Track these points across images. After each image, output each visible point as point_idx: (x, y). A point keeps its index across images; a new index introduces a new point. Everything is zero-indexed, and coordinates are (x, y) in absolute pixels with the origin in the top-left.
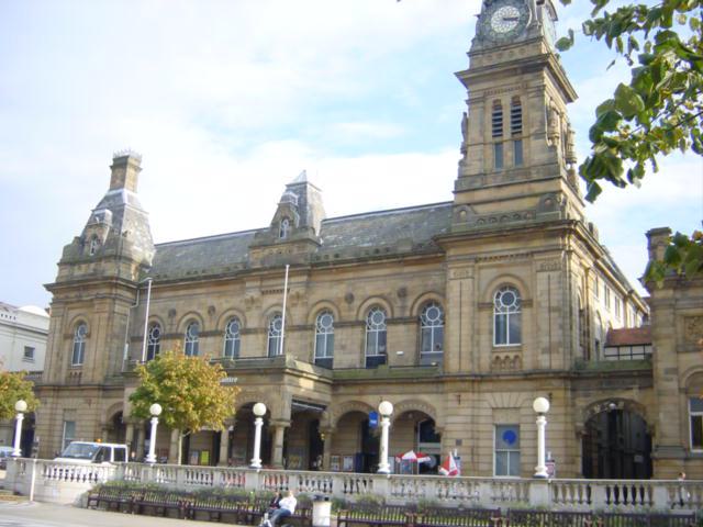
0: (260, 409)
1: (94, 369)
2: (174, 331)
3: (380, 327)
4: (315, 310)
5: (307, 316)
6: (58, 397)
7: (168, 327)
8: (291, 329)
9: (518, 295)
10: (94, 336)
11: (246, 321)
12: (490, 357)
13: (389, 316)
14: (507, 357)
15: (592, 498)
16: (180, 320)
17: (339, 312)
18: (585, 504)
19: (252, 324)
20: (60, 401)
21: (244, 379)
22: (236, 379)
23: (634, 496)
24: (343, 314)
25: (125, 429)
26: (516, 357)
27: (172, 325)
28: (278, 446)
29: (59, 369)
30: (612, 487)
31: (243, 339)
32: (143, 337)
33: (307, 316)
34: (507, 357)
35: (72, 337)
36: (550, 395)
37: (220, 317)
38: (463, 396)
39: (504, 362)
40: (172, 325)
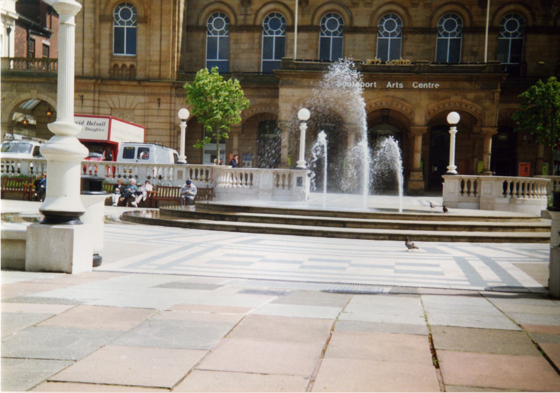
0: (454, 118)
1: (160, 62)
2: (250, 22)
3: (514, 35)
4: (440, 12)
5: (431, 18)
6: (100, 93)
7: (241, 18)
8: (301, 29)
9: (135, 10)
10: (156, 21)
11: (351, 18)
12: (110, 64)
13: (347, 22)
14: (124, 66)
15: (253, 182)
16: (258, 11)
17: (471, 17)
18: (204, 181)
19: (361, 21)
20: (103, 98)
21: (447, 84)
22: (437, 85)
23: (469, 187)
24: (475, 18)
25: (413, 138)
26: (132, 66)
27: (246, 15)
28: (285, 147)
29: (96, 59)
30: (111, 166)
31: (348, 37)
32: (485, 28)
33: (431, 18)
34: (124, 66)
35: (110, 20)
36: (159, 100)
37: (315, 12)
38: (86, 96)
39: (122, 70)
40: (246, 15)
